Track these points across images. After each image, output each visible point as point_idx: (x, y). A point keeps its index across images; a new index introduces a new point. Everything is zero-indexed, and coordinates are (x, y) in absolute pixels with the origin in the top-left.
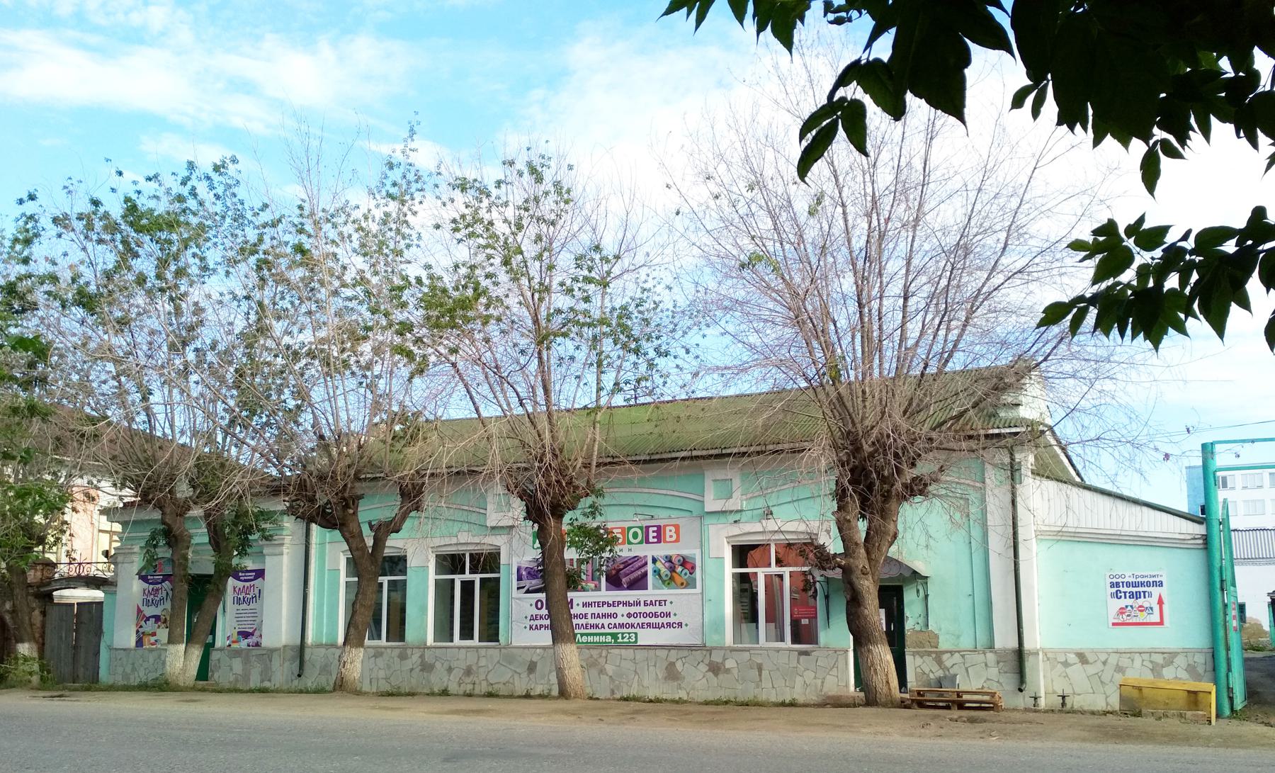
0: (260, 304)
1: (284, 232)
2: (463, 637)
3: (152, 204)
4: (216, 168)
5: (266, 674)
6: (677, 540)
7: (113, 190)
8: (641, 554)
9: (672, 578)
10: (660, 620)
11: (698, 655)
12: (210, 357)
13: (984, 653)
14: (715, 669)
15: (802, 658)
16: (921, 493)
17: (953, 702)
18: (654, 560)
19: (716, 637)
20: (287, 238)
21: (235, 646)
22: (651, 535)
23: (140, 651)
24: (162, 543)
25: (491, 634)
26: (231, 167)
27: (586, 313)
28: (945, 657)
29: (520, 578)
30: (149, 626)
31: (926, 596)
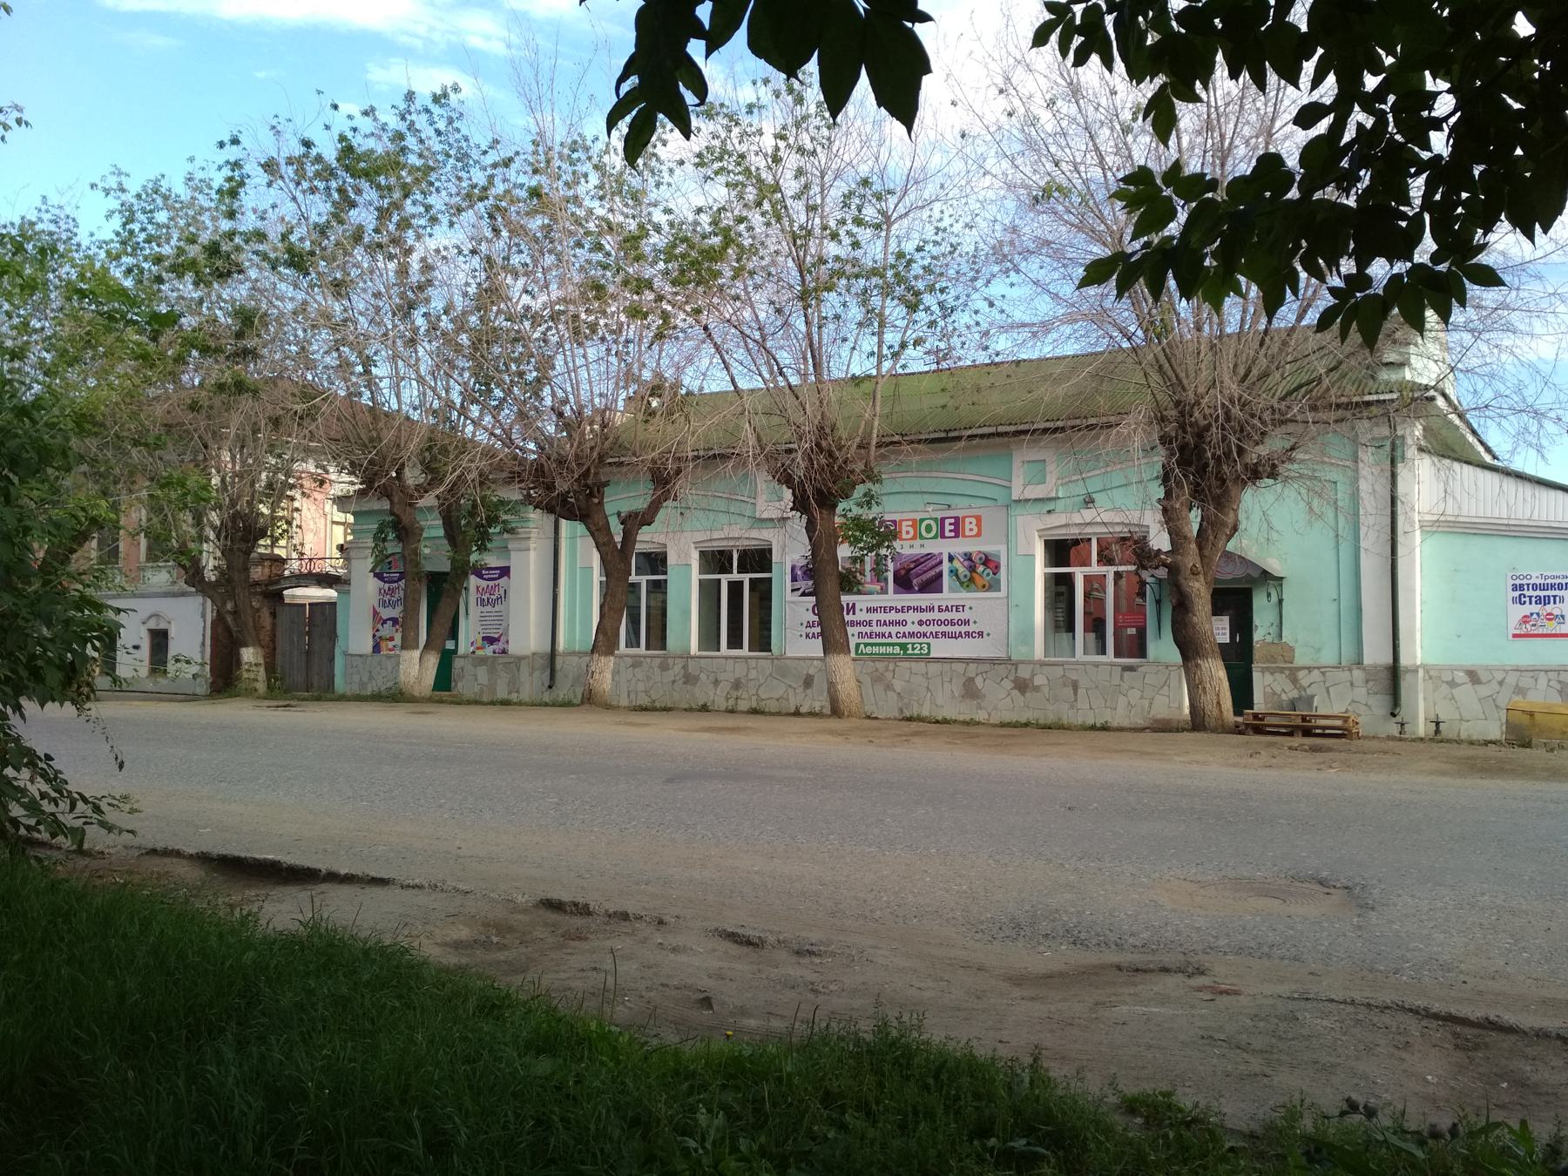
0: (489, 259)
1: (518, 172)
2: (731, 645)
3: (371, 143)
4: (436, 99)
5: (514, 686)
6: (979, 534)
7: (327, 127)
8: (935, 551)
9: (971, 580)
10: (957, 629)
11: (1002, 669)
12: (445, 323)
13: (1350, 670)
14: (1022, 686)
15: (1126, 674)
16: (1273, 475)
17: (1298, 727)
18: (951, 559)
19: (1023, 649)
20: (522, 179)
21: (479, 653)
22: (948, 528)
23: (377, 657)
24: (391, 536)
25: (762, 641)
26: (452, 96)
27: (855, 262)
28: (1301, 674)
29: (794, 579)
30: (386, 631)
31: (1280, 601)
